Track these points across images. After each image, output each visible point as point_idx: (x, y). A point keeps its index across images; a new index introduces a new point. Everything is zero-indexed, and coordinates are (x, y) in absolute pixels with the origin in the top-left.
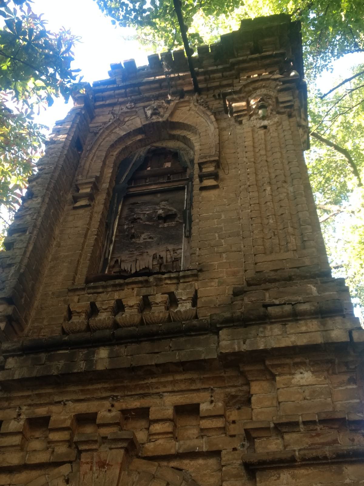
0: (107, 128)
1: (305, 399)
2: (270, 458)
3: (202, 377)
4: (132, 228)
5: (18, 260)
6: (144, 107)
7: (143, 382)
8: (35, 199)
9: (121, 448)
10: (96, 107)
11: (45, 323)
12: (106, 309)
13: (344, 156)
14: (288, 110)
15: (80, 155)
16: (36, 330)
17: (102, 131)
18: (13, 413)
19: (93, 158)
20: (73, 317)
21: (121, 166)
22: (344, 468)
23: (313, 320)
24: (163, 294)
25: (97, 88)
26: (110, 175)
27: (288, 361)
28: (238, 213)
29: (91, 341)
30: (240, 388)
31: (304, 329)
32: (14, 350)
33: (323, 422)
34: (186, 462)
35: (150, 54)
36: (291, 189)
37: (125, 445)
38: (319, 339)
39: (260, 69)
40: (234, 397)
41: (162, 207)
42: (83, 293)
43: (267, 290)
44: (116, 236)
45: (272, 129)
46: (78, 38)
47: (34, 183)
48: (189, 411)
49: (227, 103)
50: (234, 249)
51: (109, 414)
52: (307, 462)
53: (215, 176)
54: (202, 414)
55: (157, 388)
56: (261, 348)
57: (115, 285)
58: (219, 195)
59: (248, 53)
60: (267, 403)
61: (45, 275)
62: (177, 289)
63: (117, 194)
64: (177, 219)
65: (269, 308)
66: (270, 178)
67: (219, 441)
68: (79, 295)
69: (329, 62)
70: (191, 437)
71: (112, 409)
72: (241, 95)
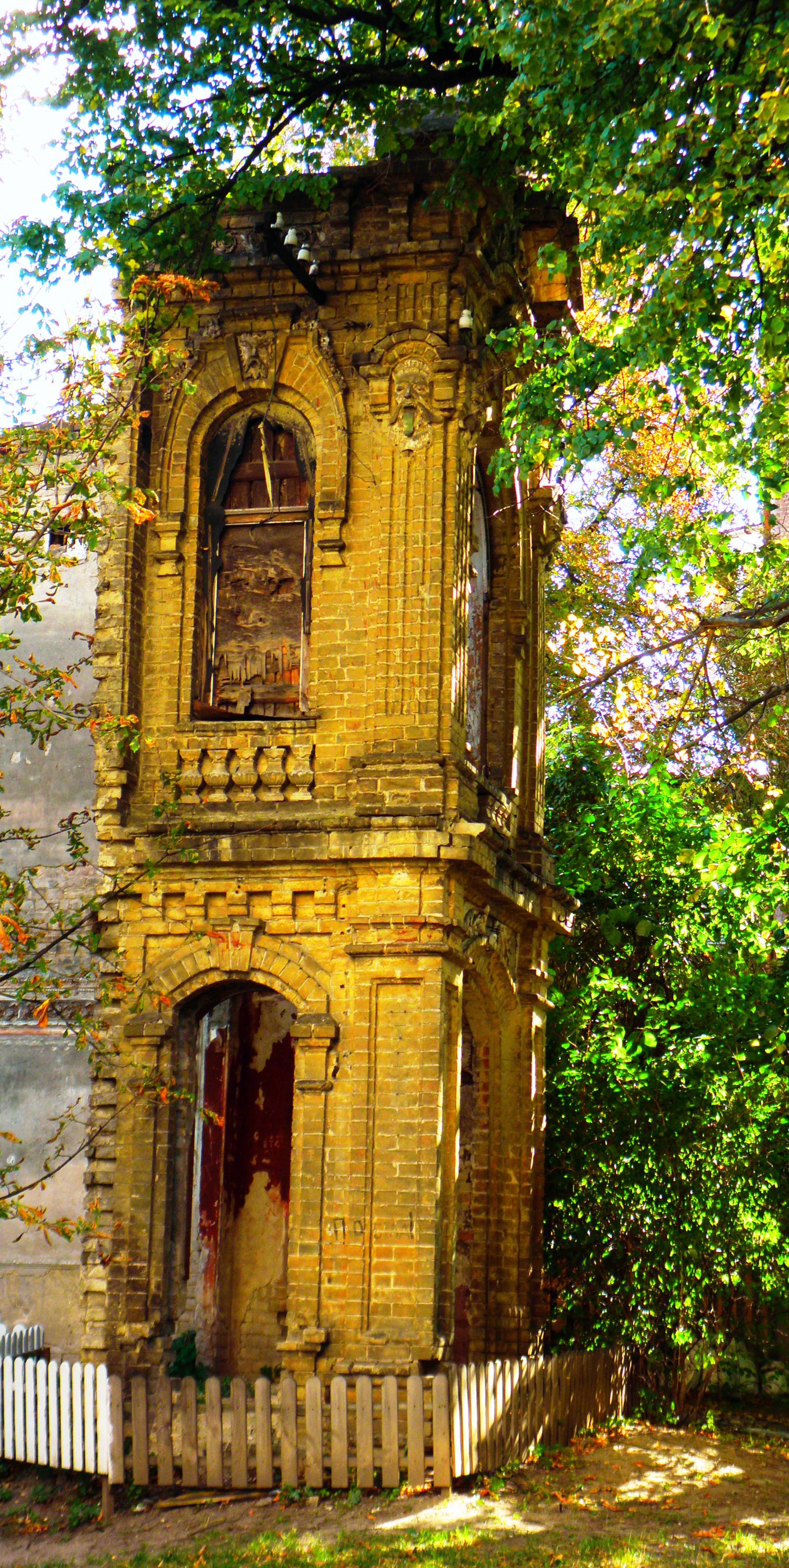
53: (341, 547)
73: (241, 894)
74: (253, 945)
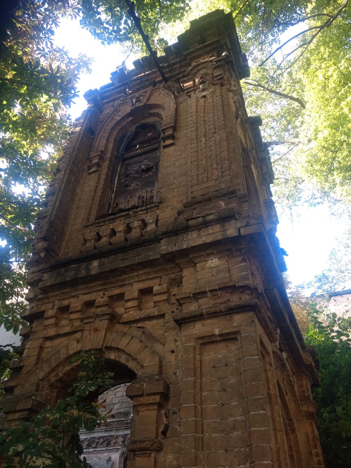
0: (109, 117)
1: (213, 276)
2: (188, 315)
3: (154, 270)
4: (126, 180)
5: (49, 213)
6: (132, 98)
7: (120, 278)
8: (61, 173)
9: (106, 319)
10: (104, 104)
11: (71, 249)
12: (106, 235)
13: (297, 103)
14: (220, 81)
15: (93, 138)
16: (65, 254)
17: (106, 119)
18: (50, 306)
19: (100, 139)
20: (87, 243)
21: (119, 141)
22: (234, 317)
23: (217, 225)
24: (138, 221)
25: (103, 91)
26: (111, 148)
27: (203, 253)
28: (186, 160)
29: (88, 258)
30: (178, 274)
31: (211, 231)
32: (46, 269)
33: (220, 289)
34: (147, 322)
35: (134, 60)
36: (218, 137)
37: (108, 317)
38: (219, 237)
39: (204, 55)
40: (174, 280)
41: (144, 163)
42: (92, 227)
43: (194, 209)
44: (117, 187)
45: (209, 97)
46: (92, 59)
47: (61, 162)
48: (147, 292)
49: (182, 85)
50: (182, 184)
51: (102, 300)
52: (211, 316)
53: (172, 137)
54: (154, 293)
55: (129, 280)
56: (185, 247)
57: (110, 220)
58: (175, 150)
59: (197, 45)
60: (192, 281)
61: (72, 219)
62: (146, 217)
63: (117, 160)
64: (154, 170)
65: (189, 221)
66: (205, 132)
67: (165, 308)
68: (90, 229)
69: (277, 37)
70: (150, 309)
71: (104, 296)
72: (189, 77)
73: (105, 298)
74: (107, 330)
